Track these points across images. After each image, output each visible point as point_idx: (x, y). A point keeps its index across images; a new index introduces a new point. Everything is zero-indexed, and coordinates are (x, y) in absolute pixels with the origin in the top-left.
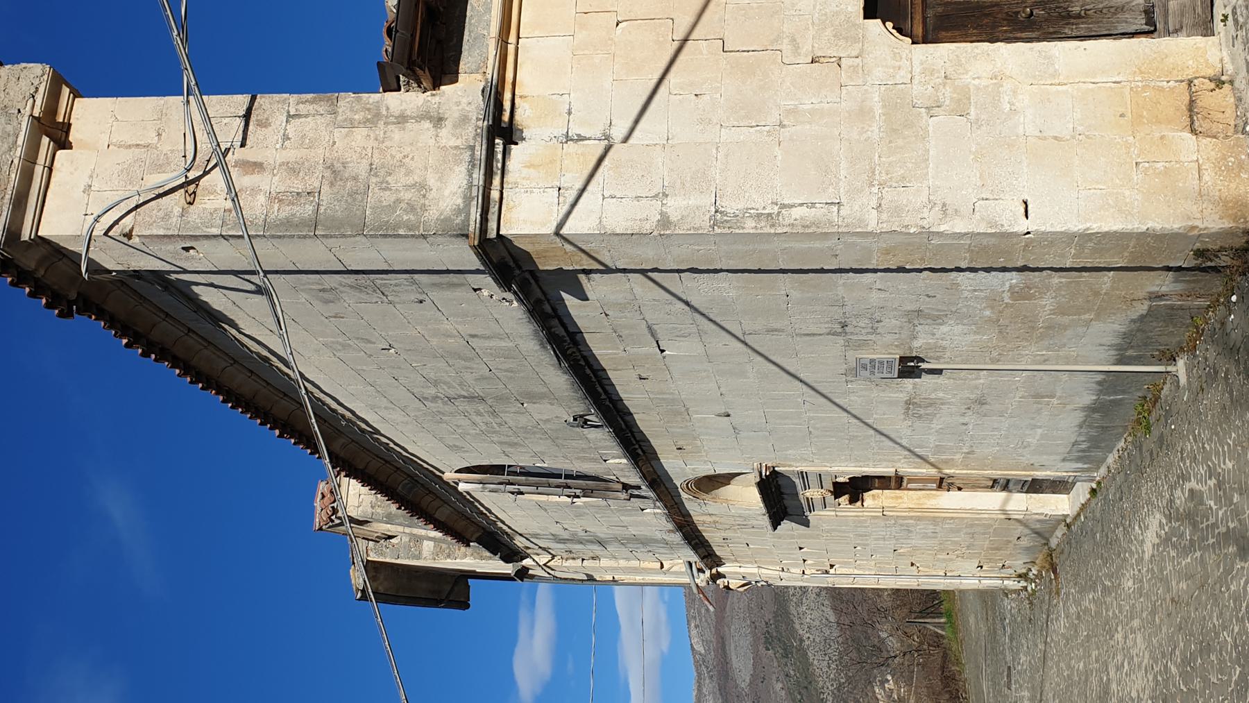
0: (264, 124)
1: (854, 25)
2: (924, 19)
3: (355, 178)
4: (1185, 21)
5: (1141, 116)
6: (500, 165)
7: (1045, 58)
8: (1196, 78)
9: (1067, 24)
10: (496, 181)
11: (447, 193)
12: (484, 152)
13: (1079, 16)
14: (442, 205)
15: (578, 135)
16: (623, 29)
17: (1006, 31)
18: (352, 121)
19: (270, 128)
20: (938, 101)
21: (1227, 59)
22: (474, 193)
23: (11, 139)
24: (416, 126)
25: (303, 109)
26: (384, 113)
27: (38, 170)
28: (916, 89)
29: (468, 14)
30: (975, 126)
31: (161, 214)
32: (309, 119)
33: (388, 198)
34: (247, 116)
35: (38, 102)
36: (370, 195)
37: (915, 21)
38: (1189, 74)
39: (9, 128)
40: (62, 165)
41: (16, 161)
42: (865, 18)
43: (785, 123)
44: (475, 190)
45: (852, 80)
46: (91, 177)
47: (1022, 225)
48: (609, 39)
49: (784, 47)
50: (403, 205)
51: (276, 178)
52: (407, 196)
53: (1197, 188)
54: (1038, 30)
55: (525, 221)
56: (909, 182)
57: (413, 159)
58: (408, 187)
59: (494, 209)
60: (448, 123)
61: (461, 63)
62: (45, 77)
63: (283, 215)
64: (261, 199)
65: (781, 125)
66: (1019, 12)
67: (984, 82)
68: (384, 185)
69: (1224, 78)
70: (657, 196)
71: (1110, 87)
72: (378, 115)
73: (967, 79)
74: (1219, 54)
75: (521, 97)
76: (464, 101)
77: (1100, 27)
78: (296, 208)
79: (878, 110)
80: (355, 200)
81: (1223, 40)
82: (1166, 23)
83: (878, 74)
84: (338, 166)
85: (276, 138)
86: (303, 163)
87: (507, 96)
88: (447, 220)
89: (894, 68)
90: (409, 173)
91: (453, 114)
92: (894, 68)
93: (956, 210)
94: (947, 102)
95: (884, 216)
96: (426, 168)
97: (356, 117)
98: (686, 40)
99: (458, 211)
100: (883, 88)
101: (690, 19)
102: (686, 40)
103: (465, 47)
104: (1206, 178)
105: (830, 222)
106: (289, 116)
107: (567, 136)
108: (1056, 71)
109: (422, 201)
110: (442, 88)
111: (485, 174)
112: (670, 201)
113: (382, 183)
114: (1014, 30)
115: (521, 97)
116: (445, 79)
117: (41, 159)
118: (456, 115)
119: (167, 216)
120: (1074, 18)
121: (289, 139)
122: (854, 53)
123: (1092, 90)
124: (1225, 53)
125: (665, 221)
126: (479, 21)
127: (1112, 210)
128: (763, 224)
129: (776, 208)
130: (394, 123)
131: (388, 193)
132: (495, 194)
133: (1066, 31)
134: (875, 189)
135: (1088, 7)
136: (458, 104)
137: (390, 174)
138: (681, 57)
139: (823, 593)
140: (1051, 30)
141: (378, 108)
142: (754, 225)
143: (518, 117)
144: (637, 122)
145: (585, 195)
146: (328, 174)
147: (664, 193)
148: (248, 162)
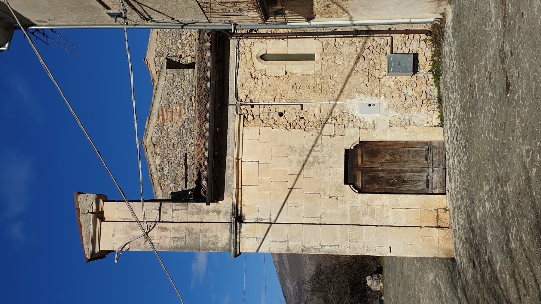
0: (165, 213)
1: (341, 186)
2: (362, 181)
3: (196, 233)
4: (438, 186)
5: (423, 220)
6: (239, 231)
7: (396, 200)
8: (439, 208)
9: (403, 185)
10: (238, 236)
11: (224, 239)
12: (234, 229)
13: (407, 182)
14: (223, 242)
15: (261, 218)
16: (273, 184)
17: (385, 186)
18: (192, 212)
19: (167, 214)
20: (366, 212)
21: (448, 203)
22: (232, 242)
23: (88, 222)
24: (212, 214)
25: (177, 208)
26: (202, 210)
27: (97, 230)
28: (359, 208)
29: (226, 177)
30: (376, 221)
31: (138, 244)
32: (179, 211)
33: (206, 240)
34: (160, 210)
35: (94, 207)
36: (201, 239)
37: (359, 182)
38: (437, 207)
39: (87, 218)
40: (104, 227)
41: (91, 229)
42: (345, 184)
43: (322, 217)
44: (232, 241)
45: (341, 204)
46: (114, 231)
47: (389, 255)
48: (269, 187)
49: (321, 193)
50: (211, 242)
51: (172, 233)
52: (212, 239)
53: (437, 245)
54: (395, 186)
55: (247, 248)
56: (358, 240)
57: (213, 227)
58: (212, 237)
59: (238, 245)
60: (222, 213)
61: (225, 194)
62: (95, 198)
63: (175, 245)
64: (168, 240)
65: (321, 218)
66: (389, 180)
67: (379, 207)
68: (205, 236)
69: (447, 209)
70: (286, 241)
71: (415, 211)
72: (200, 210)
73: (374, 205)
74: (446, 201)
75: (243, 205)
76: (226, 206)
77: (413, 186)
78: (179, 243)
79: (349, 215)
80: (196, 240)
81: (447, 197)
82: (432, 186)
83: (349, 203)
84: (190, 229)
85: (169, 217)
86: (180, 228)
87: (239, 206)
88: (224, 247)
89: (353, 201)
90: (212, 232)
91: (223, 211)
92: (353, 201)
93: (371, 250)
94: (368, 213)
95: (351, 250)
96: (217, 231)
97: (194, 211)
98: (292, 189)
99: (227, 245)
100: (350, 207)
101: (293, 182)
102: (292, 189)
103: (225, 188)
104: (440, 242)
105: (336, 251)
106: (173, 210)
107: (258, 219)
108: (399, 204)
109: (216, 241)
110: (219, 202)
111: (235, 236)
112: (290, 243)
113: (204, 235)
114: (388, 186)
115: (243, 205)
116: (220, 199)
117: (98, 226)
118: (224, 211)
119: (140, 245)
120: (406, 183)
121: (174, 218)
122: (341, 196)
123: (409, 211)
124: (448, 201)
125: (288, 249)
126: (229, 180)
127: (414, 251)
128: (317, 251)
129: (320, 246)
130: (205, 213)
131: (206, 238)
132: (238, 240)
133: (403, 187)
134: (348, 242)
135: (409, 180)
136: (225, 207)
137: (206, 232)
138: (291, 194)
139: (422, 186)
140: (399, 186)
141: (200, 208)
142: (314, 251)
143: (243, 212)
144: (278, 215)
145: (265, 240)
146: (187, 232)
147: (288, 240)
148: (163, 227)
